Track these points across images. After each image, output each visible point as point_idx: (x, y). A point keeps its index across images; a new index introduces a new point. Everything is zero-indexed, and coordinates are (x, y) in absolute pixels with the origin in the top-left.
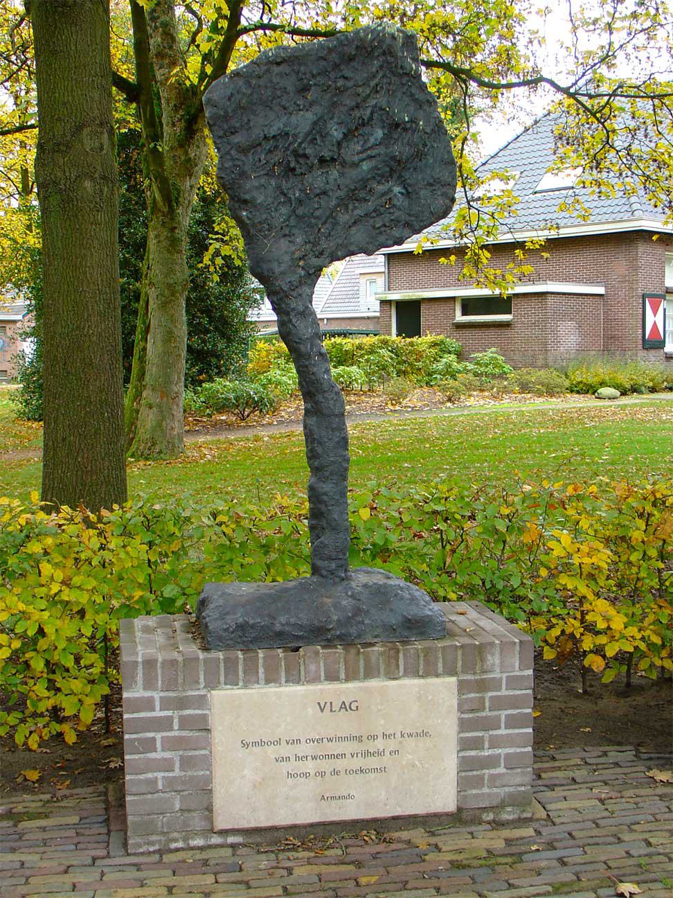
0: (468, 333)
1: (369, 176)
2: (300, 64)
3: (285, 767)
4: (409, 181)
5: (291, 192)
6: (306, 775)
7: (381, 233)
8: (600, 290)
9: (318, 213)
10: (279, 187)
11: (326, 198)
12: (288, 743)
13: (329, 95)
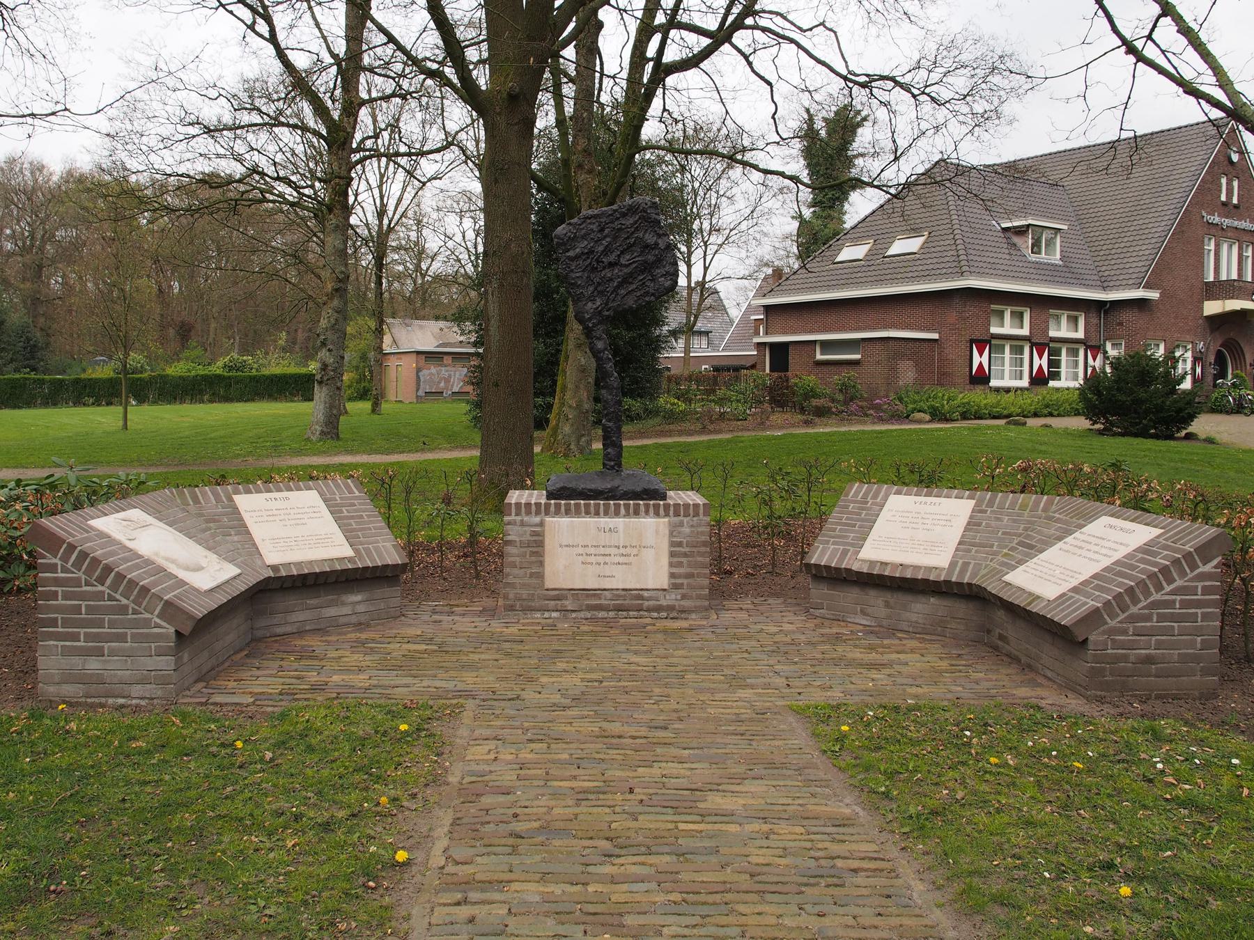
0: (825, 369)
8: (935, 336)
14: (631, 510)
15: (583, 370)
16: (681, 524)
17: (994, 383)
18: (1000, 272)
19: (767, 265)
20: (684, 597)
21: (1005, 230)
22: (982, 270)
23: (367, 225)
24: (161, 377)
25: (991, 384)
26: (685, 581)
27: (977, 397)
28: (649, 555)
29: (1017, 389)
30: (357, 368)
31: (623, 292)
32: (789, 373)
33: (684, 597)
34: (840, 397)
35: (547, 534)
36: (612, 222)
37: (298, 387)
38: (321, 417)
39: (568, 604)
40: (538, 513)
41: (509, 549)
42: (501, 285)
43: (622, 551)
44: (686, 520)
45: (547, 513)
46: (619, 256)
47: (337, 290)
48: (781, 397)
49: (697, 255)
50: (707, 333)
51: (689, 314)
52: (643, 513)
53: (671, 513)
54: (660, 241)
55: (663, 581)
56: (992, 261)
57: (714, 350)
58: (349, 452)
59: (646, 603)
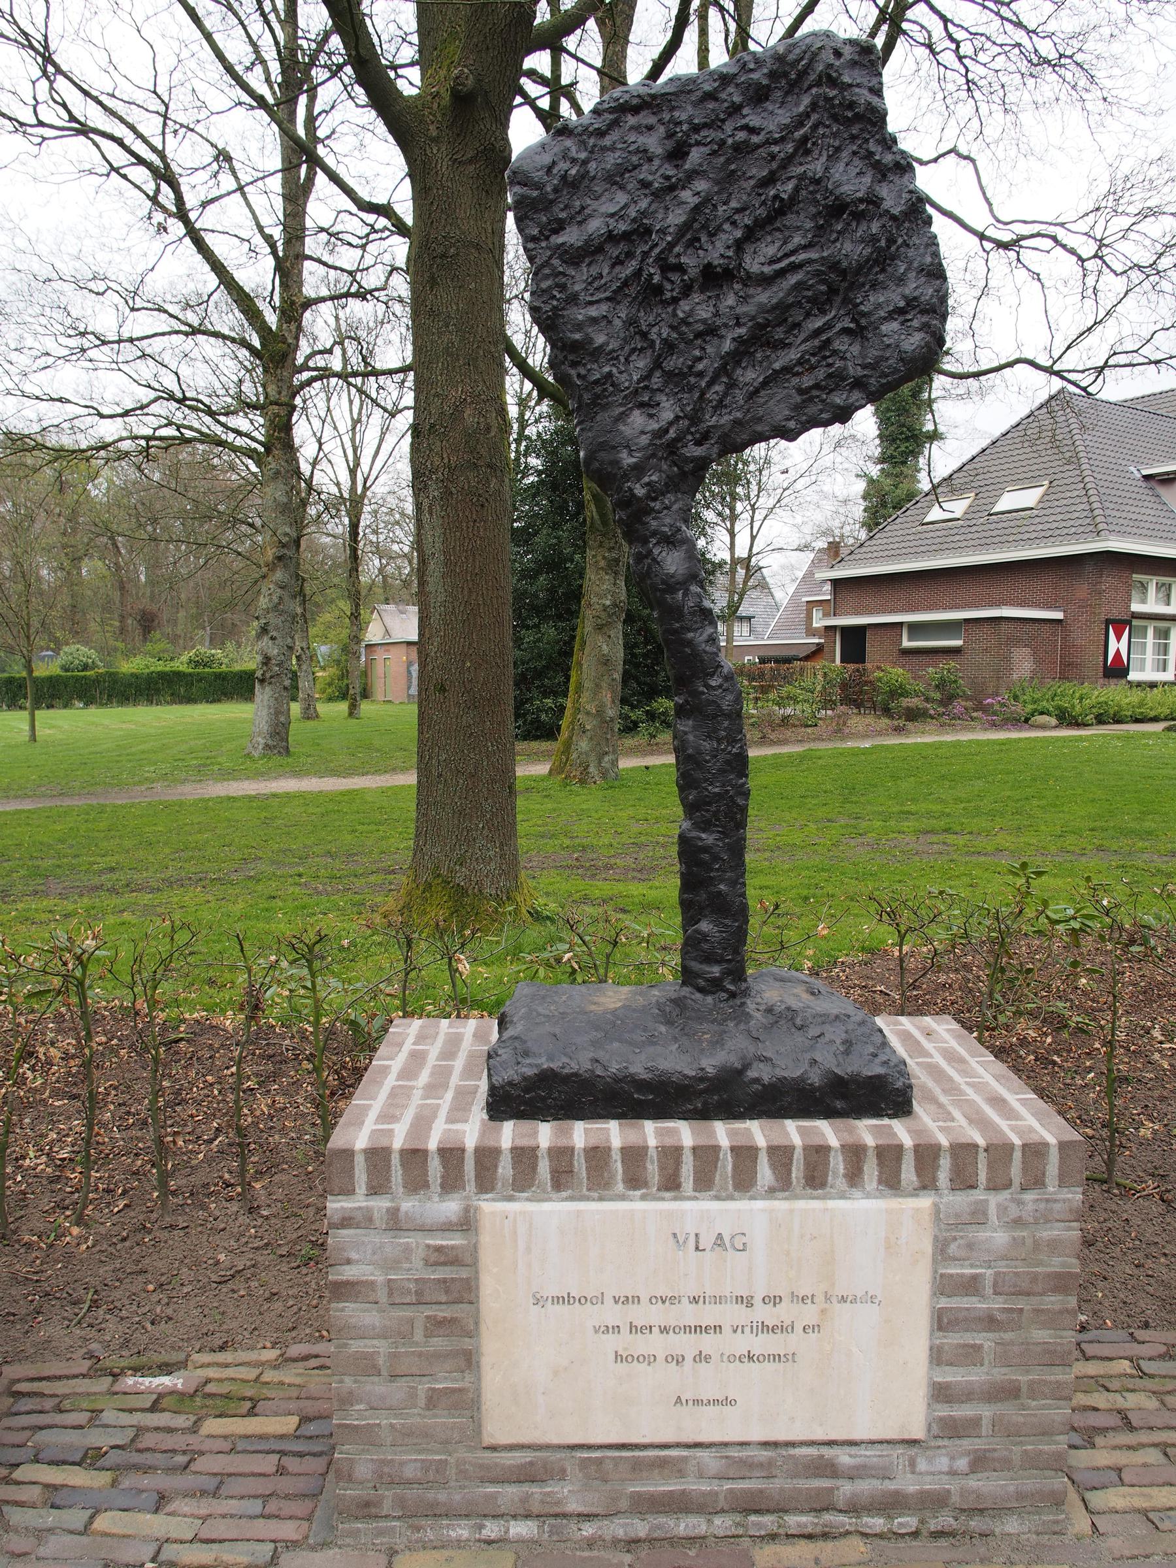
0: (914, 659)
1: (791, 300)
2: (673, 109)
3: (612, 1342)
4: (862, 308)
5: (655, 330)
6: (650, 1359)
7: (811, 399)
8: (1059, 615)
9: (700, 367)
10: (631, 322)
11: (716, 341)
12: (616, 1302)
13: (722, 159)
14: (797, 1171)
15: (606, 662)
16: (978, 1217)
17: (1133, 676)
18: (1145, 532)
19: (824, 534)
20: (979, 1462)
21: (1147, 478)
22: (1123, 529)
23: (338, 484)
24: (111, 674)
25: (1129, 678)
26: (986, 1412)
27: (1113, 694)
28: (857, 1327)
29: (1165, 684)
30: (338, 662)
31: (750, 376)
32: (868, 665)
33: (979, 1462)
34: (937, 696)
35: (486, 1258)
36: (714, 123)
37: (238, 686)
38: (265, 727)
39: (570, 1494)
40: (452, 1183)
41: (350, 1312)
42: (447, 494)
43: (762, 1313)
44: (994, 1200)
45: (486, 1182)
46: (739, 246)
47: (280, 558)
48: (856, 695)
49: (742, 527)
50: (749, 618)
51: (731, 592)
52: (841, 1183)
53: (943, 1176)
54: (884, 191)
55: (910, 1415)
56: (1134, 517)
57: (757, 639)
58: (297, 774)
59: (846, 1489)
